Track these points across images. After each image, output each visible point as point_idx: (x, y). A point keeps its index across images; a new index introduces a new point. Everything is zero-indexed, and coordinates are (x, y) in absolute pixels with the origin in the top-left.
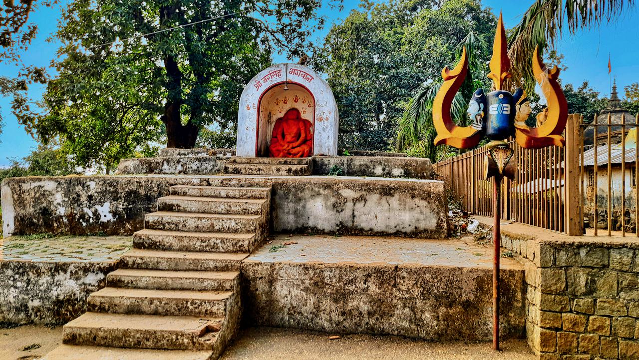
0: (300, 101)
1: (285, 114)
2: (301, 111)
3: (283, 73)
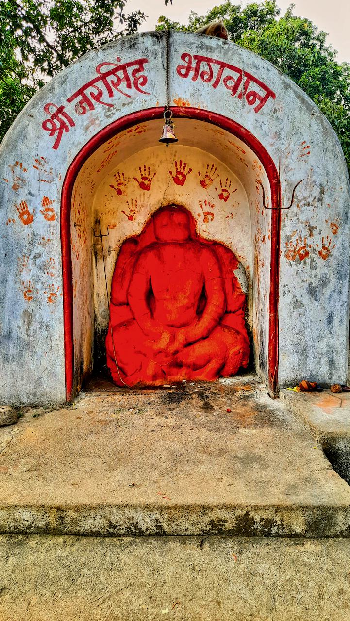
0: (192, 181)
1: (148, 224)
2: (197, 211)
3: (154, 72)
